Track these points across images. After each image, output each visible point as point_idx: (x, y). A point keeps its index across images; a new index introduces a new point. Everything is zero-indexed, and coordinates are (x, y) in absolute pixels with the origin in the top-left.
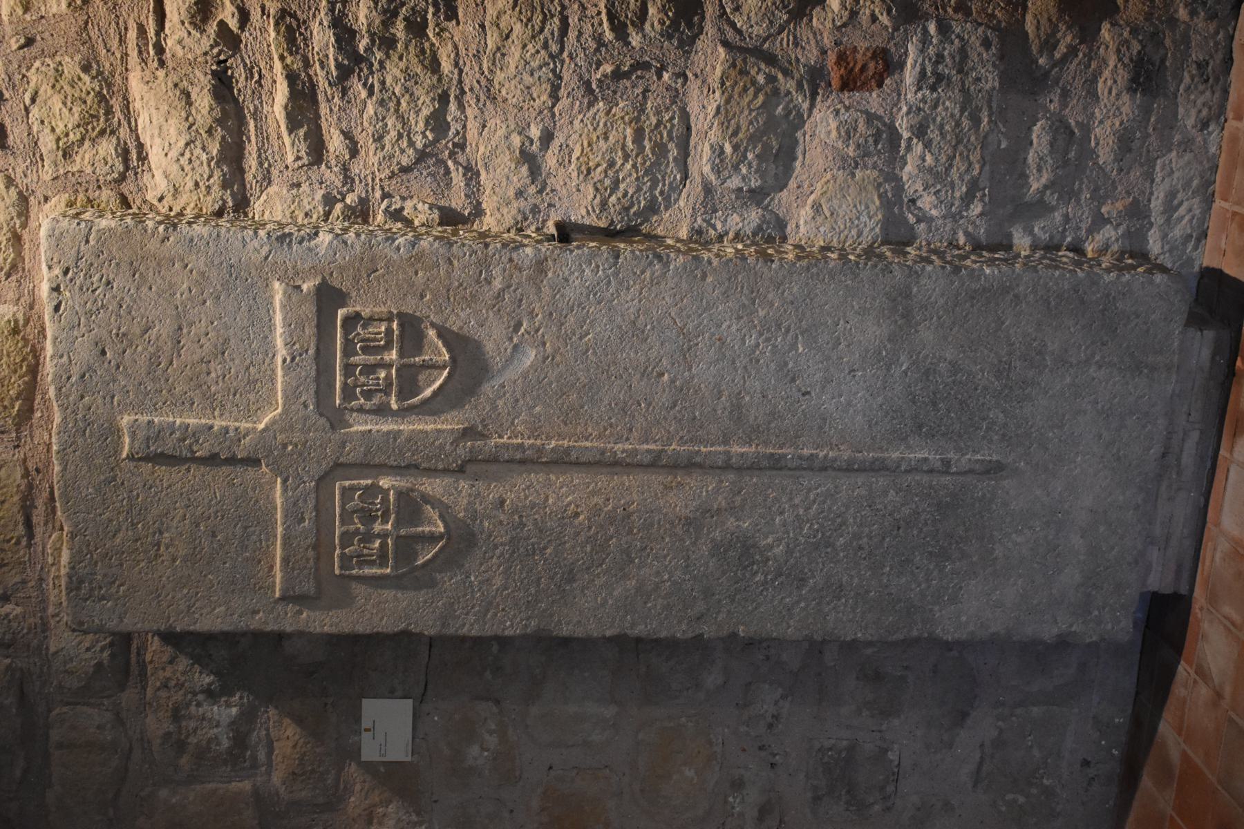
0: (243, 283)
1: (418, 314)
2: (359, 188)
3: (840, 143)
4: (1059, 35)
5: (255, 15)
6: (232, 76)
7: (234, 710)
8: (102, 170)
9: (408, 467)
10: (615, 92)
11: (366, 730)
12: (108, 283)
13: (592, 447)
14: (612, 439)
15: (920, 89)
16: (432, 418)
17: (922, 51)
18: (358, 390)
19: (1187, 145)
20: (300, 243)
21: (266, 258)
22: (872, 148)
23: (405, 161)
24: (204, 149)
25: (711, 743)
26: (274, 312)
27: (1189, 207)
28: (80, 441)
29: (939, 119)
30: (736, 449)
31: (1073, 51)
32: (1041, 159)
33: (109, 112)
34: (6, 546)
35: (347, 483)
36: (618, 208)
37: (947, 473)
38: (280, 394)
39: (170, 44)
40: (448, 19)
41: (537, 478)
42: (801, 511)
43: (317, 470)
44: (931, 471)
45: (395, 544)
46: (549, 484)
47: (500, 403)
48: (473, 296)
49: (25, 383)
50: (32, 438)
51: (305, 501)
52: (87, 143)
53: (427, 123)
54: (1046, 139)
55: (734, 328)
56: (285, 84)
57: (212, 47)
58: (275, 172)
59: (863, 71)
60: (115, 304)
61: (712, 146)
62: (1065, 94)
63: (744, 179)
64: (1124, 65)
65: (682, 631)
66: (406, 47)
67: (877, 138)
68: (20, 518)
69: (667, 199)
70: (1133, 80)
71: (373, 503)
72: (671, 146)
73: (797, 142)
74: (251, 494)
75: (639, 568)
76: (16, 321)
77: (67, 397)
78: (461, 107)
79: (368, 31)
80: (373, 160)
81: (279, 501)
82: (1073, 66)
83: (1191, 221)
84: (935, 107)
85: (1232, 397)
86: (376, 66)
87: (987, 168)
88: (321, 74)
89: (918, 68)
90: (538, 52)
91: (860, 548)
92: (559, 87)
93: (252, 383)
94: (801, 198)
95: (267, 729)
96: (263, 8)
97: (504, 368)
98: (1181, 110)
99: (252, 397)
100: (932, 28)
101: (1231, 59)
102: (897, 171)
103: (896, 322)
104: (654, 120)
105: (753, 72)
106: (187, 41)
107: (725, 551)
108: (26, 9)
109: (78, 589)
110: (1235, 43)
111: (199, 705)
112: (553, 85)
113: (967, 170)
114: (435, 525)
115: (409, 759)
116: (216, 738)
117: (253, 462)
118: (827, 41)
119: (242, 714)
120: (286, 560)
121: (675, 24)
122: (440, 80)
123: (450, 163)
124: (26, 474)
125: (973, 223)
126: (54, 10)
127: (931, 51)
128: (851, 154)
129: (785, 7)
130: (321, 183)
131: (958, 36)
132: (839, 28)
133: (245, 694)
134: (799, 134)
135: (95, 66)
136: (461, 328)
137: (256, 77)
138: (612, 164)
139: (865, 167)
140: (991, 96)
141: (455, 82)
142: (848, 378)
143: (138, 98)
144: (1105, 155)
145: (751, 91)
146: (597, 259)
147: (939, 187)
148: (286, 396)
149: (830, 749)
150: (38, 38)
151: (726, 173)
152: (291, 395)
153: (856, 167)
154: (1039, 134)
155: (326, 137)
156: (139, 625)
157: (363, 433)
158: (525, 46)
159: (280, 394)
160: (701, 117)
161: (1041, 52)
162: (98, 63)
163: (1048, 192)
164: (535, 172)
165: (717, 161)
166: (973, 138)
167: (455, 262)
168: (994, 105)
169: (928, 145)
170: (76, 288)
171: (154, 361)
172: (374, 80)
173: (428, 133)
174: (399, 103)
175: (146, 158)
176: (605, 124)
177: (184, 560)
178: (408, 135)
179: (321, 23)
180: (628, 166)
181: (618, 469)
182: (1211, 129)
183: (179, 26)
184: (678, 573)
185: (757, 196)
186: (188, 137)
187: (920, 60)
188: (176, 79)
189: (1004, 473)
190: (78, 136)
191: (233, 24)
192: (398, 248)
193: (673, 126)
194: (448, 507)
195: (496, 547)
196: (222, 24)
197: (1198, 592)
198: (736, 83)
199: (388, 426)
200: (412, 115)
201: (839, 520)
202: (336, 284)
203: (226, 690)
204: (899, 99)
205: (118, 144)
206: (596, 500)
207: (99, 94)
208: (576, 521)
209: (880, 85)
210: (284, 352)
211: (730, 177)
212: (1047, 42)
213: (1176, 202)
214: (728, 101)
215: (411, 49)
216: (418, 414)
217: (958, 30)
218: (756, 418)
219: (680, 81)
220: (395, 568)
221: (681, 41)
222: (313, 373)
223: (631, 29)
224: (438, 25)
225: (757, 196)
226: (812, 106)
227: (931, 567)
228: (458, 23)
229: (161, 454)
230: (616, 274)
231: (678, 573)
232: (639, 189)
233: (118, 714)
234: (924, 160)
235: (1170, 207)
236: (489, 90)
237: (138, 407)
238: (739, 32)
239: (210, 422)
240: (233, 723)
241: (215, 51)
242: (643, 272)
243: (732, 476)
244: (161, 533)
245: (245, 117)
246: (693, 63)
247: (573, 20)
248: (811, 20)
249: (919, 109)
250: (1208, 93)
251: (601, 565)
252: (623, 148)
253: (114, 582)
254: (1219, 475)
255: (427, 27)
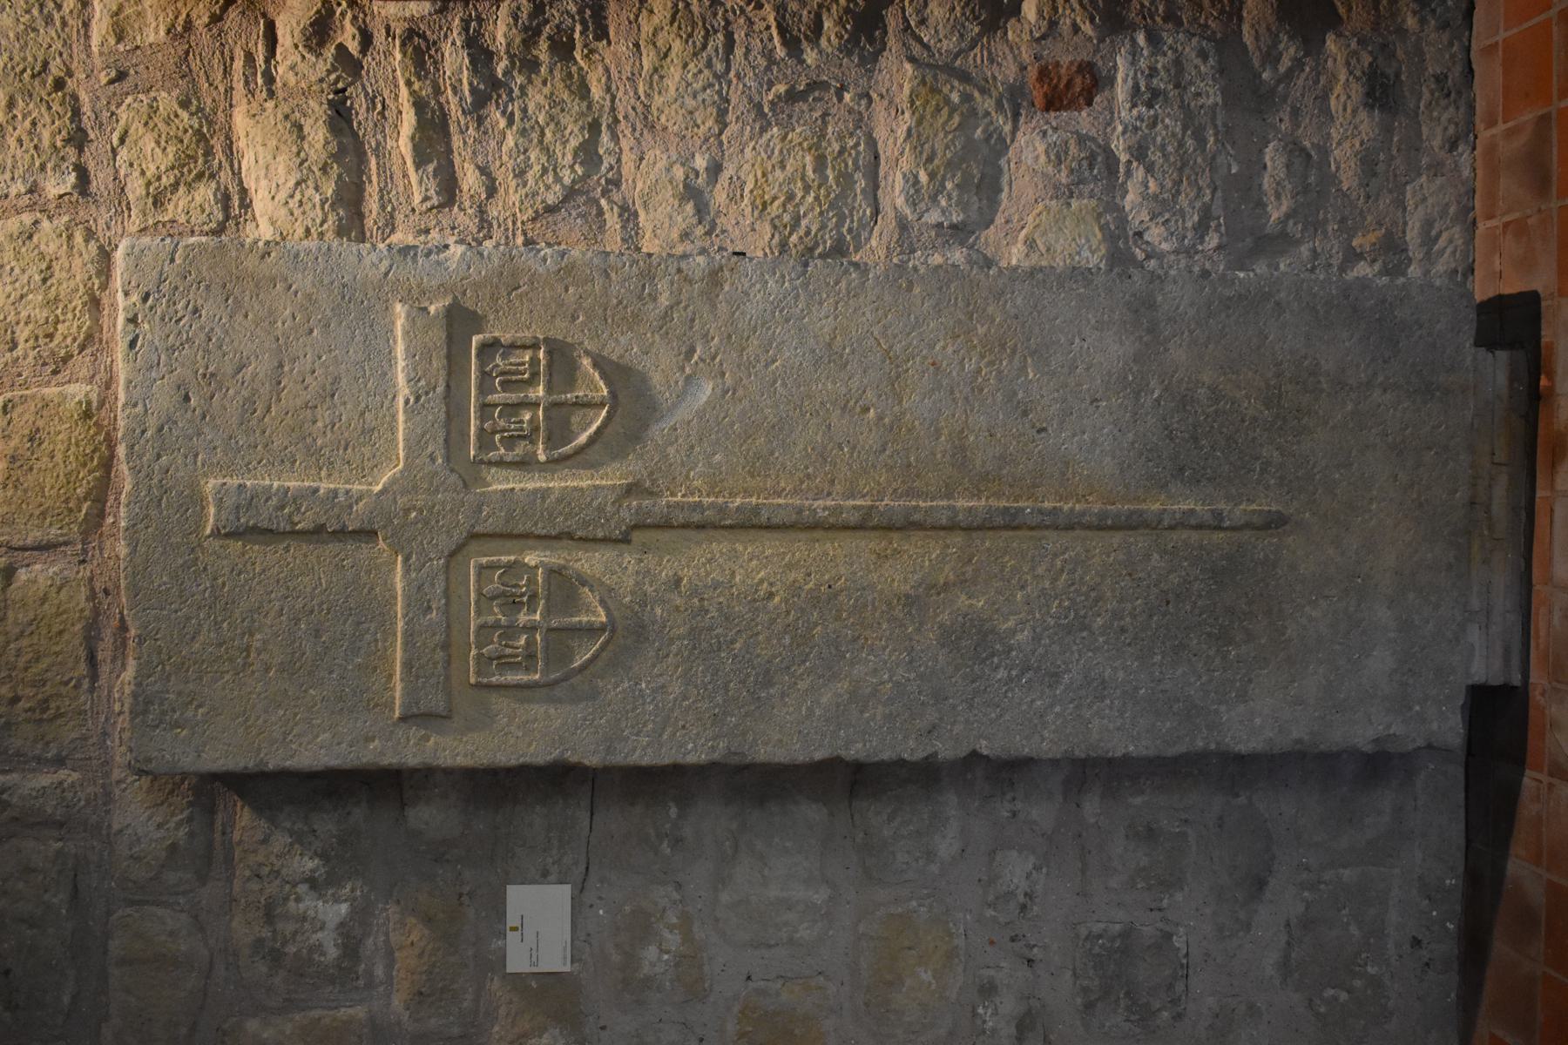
0: (359, 305)
1: (569, 340)
2: (497, 234)
3: (1050, 168)
4: (1281, 46)
5: (379, 38)
6: (352, 107)
7: (344, 908)
8: (197, 218)
9: (558, 537)
10: (790, 117)
11: (512, 929)
12: (196, 311)
13: (787, 505)
14: (810, 495)
15: (1134, 106)
16: (588, 473)
17: (1132, 64)
18: (497, 437)
19: (1436, 168)
20: (428, 255)
21: (386, 274)
22: (1087, 174)
23: (551, 199)
24: (317, 189)
25: (951, 935)
26: (395, 342)
27: (1450, 237)
28: (153, 513)
29: (1159, 139)
30: (962, 503)
31: (1298, 64)
32: (1278, 184)
33: (209, 153)
34: (63, 690)
35: (484, 560)
36: (800, 248)
37: (1219, 528)
38: (401, 446)
39: (281, 71)
40: (598, 38)
41: (719, 546)
42: (1047, 584)
43: (446, 543)
44: (1199, 527)
45: (545, 639)
46: (734, 556)
47: (671, 450)
48: (635, 316)
49: (96, 479)
50: (101, 550)
51: (433, 585)
52: (182, 189)
53: (575, 155)
54: (1281, 161)
55: (950, 350)
56: (412, 112)
57: (329, 72)
58: (399, 217)
59: (1070, 89)
60: (202, 336)
61: (904, 176)
62: (1295, 112)
63: (943, 212)
64: (1358, 79)
65: (912, 750)
66: (551, 71)
67: (1092, 160)
68: (82, 653)
69: (856, 238)
70: (1368, 95)
71: (516, 586)
72: (858, 176)
73: (1000, 170)
74: (364, 578)
75: (852, 664)
76: (89, 403)
77: (140, 457)
78: (615, 138)
79: (507, 52)
80: (514, 198)
81: (399, 586)
82: (1300, 82)
83: (1454, 252)
84: (1154, 124)
85: (1541, 425)
86: (517, 92)
87: (1219, 194)
88: (453, 100)
89: (1130, 82)
90: (700, 71)
91: (1123, 630)
92: (727, 111)
93: (367, 432)
94: (1011, 236)
95: (387, 934)
96: (388, 29)
97: (675, 406)
98: (1425, 130)
99: (367, 451)
100: (1141, 39)
101: (1471, 71)
102: (1118, 200)
103: (1141, 337)
104: (836, 147)
105: (946, 90)
106: (301, 67)
107: (959, 638)
108: (120, 39)
109: (145, 712)
110: (1473, 54)
111: (298, 900)
112: (719, 109)
113: (1197, 197)
114: (594, 613)
115: (567, 968)
116: (320, 945)
117: (367, 534)
118: (1026, 56)
119: (353, 911)
120: (408, 665)
121: (854, 40)
122: (589, 107)
123: (603, 202)
124: (92, 596)
125: (1210, 258)
126: (151, 39)
127: (1143, 64)
128: (1064, 181)
129: (976, 18)
130: (453, 228)
131: (1171, 48)
132: (1038, 40)
133: (359, 883)
134: (1003, 162)
135: (195, 102)
136: (621, 357)
137: (379, 107)
138: (790, 197)
139: (1081, 196)
140: (1214, 112)
141: (607, 109)
142: (1091, 409)
143: (242, 134)
144: (1348, 179)
145: (945, 112)
146: (782, 267)
147: (1167, 216)
148: (408, 447)
149: (1100, 936)
150: (132, 72)
151: (923, 206)
152: (415, 445)
153: (1071, 196)
154: (1273, 156)
155: (459, 174)
156: (221, 762)
157: (503, 492)
158: (685, 66)
159: (401, 446)
160: (891, 141)
161: (1263, 65)
162: (198, 99)
163: (1291, 223)
164: (701, 211)
165: (912, 191)
166: (1199, 160)
167: (613, 275)
168: (1219, 123)
169: (1149, 169)
170: (157, 318)
171: (249, 405)
172: (515, 108)
173: (577, 167)
174: (543, 134)
175: (250, 205)
176: (781, 151)
177: (282, 669)
178: (554, 170)
179: (453, 44)
180: (810, 199)
181: (818, 534)
182: (1460, 149)
183: (292, 50)
184: (900, 671)
185: (959, 233)
186: (299, 176)
187: (1131, 74)
188: (287, 110)
189: (1287, 527)
190: (172, 180)
191: (353, 47)
192: (544, 260)
193: (858, 153)
194: (611, 590)
195: (672, 641)
196: (341, 48)
197: (1534, 678)
198: (927, 102)
199: (533, 483)
200: (559, 147)
201: (1093, 594)
202: (470, 305)
203: (333, 880)
204: (1112, 118)
205: (218, 189)
206: (792, 576)
207: (199, 132)
208: (771, 605)
209: (1089, 103)
210: (407, 391)
211: (927, 210)
212: (1268, 54)
213: (1434, 233)
214: (919, 122)
215: (557, 73)
216: (570, 468)
217: (1170, 41)
218: (984, 462)
219: (864, 102)
220: (545, 672)
221: (861, 58)
222: (443, 416)
223: (805, 44)
224: (586, 46)
225: (959, 233)
226: (1015, 129)
227: (1211, 653)
228: (609, 43)
229: (249, 530)
230: (806, 285)
231: (900, 671)
232: (823, 227)
233: (196, 917)
234: (1147, 187)
235: (1429, 240)
236: (646, 118)
237: (228, 469)
238: (926, 47)
239: (315, 485)
240: (342, 924)
241: (333, 77)
242: (837, 283)
243: (958, 539)
244: (252, 635)
245: (365, 153)
246: (877, 82)
247: (739, 36)
248: (1006, 33)
249: (1136, 129)
250: (1452, 109)
251: (804, 662)
252: (803, 179)
253: (191, 703)
254: (1541, 520)
255: (574, 48)
